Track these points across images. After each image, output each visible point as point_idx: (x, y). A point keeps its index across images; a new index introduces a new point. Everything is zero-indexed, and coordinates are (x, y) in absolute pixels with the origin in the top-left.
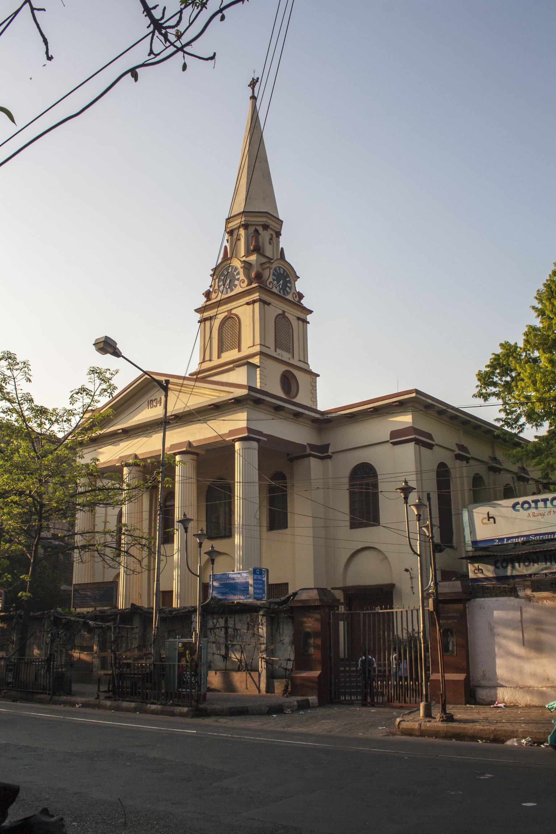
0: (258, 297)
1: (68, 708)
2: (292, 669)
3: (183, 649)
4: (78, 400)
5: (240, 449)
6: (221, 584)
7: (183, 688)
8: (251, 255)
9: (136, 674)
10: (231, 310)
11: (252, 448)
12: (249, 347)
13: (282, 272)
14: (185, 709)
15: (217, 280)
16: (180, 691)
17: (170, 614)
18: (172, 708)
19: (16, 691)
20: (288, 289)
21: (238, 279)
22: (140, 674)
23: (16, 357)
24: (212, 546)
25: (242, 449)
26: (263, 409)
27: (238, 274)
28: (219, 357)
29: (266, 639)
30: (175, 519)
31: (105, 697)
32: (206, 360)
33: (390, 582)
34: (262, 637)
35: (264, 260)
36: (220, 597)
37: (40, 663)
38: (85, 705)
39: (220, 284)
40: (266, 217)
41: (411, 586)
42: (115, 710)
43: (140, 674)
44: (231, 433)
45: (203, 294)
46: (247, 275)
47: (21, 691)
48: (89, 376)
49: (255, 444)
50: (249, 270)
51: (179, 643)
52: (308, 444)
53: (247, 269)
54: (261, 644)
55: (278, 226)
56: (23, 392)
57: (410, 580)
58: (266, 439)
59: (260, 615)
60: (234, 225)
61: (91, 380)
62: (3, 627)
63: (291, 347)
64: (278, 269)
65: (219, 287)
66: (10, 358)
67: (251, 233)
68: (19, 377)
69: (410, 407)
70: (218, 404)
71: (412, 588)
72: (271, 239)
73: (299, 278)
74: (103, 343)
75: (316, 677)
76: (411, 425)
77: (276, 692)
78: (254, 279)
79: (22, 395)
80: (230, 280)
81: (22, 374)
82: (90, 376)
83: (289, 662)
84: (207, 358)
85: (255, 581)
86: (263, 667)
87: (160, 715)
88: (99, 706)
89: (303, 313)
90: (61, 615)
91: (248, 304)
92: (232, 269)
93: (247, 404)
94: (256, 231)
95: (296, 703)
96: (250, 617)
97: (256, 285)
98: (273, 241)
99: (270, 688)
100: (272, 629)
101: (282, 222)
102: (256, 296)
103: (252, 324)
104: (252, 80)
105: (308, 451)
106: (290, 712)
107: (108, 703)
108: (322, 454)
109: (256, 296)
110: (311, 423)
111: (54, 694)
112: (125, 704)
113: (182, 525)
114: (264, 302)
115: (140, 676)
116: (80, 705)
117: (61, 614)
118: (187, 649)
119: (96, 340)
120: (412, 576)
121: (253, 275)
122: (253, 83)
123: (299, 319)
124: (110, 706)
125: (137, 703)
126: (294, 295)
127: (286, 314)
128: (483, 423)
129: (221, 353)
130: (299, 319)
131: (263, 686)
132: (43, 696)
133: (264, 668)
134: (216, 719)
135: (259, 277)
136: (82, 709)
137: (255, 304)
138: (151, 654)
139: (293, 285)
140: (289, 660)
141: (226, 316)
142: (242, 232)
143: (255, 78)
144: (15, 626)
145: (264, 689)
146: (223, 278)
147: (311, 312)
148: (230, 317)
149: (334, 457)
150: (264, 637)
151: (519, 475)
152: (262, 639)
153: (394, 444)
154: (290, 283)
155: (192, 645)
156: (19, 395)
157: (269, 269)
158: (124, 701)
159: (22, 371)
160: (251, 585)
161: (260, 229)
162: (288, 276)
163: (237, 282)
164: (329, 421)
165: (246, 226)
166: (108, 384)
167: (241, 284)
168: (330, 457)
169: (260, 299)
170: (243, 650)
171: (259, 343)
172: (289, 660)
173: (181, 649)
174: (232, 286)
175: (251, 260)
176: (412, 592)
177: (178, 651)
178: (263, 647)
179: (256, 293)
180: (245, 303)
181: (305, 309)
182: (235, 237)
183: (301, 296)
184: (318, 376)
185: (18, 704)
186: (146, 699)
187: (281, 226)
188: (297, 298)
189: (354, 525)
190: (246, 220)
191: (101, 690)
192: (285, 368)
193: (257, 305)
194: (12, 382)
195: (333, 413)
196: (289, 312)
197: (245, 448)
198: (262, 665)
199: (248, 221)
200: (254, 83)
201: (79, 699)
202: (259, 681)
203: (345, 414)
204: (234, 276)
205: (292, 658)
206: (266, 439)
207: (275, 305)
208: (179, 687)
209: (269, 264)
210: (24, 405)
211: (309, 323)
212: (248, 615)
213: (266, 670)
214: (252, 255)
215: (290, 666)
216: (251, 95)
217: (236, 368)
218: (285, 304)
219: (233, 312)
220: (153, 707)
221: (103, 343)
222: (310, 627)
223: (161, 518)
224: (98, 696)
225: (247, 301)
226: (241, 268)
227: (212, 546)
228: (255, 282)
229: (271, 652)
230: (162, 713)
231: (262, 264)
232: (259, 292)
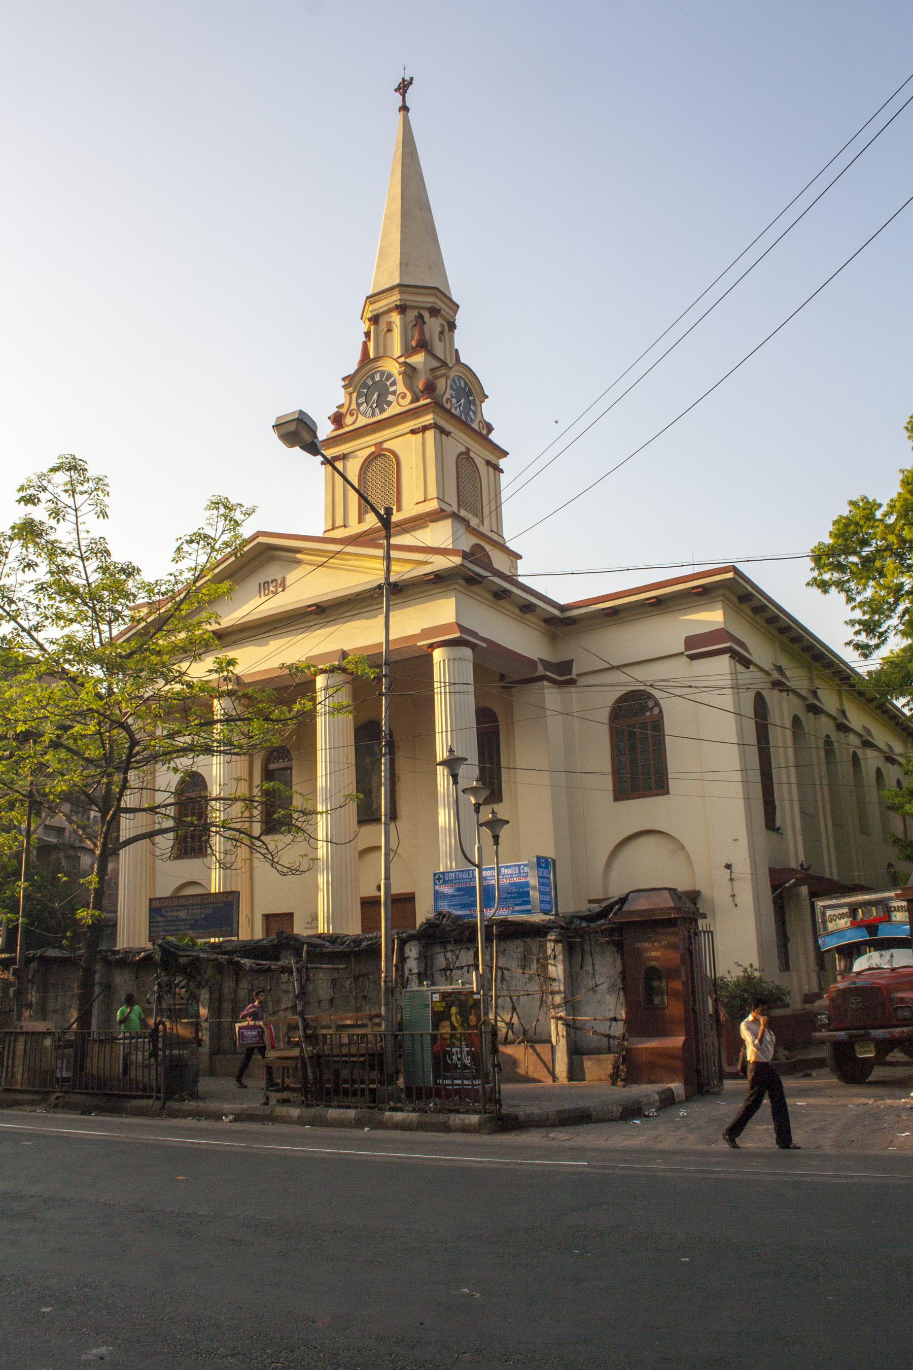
0: (432, 421)
1: (204, 1124)
3: (444, 1004)
4: (188, 556)
5: (444, 660)
6: (458, 890)
7: (446, 1078)
9: (344, 1056)
11: (465, 660)
12: (417, 503)
13: (463, 385)
14: (474, 1119)
15: (354, 395)
16: (439, 1084)
18: (442, 1117)
21: (394, 393)
22: (363, 1055)
23: (86, 466)
27: (394, 383)
28: (360, 521)
29: (564, 984)
31: (278, 1101)
34: (554, 980)
35: (435, 364)
36: (459, 913)
37: (127, 1041)
39: (360, 401)
41: (729, 892)
42: (313, 1126)
44: (426, 633)
45: (329, 418)
46: (410, 386)
48: (209, 513)
49: (468, 652)
50: (411, 378)
51: (432, 993)
52: (539, 659)
53: (408, 376)
54: (552, 993)
56: (90, 536)
58: (484, 645)
59: (550, 940)
60: (381, 308)
62: (7, 980)
63: (479, 508)
64: (456, 379)
65: (359, 405)
66: (75, 468)
67: (412, 321)
68: (85, 509)
71: (733, 896)
72: (442, 333)
73: (487, 397)
74: (295, 423)
75: (678, 1048)
76: (722, 626)
77: (587, 1078)
78: (422, 392)
79: (88, 541)
80: (379, 395)
81: (90, 502)
82: (211, 512)
84: (340, 522)
85: (541, 880)
86: (560, 1034)
87: (416, 1130)
88: (271, 1119)
89: (495, 455)
91: (413, 432)
92: (382, 377)
93: (457, 583)
94: (420, 317)
95: (657, 1097)
97: (428, 401)
98: (444, 336)
99: (575, 1073)
100: (571, 966)
101: (458, 306)
102: (428, 419)
103: (422, 465)
104: (401, 81)
105: (541, 671)
106: (656, 1114)
107: (295, 1112)
108: (561, 676)
109: (428, 419)
110: (542, 624)
111: (169, 1097)
112: (333, 1113)
115: (362, 1059)
116: (231, 1117)
118: (452, 1005)
119: (278, 418)
121: (421, 385)
122: (404, 87)
123: (488, 463)
125: (359, 1110)
127: (472, 454)
129: (364, 514)
130: (488, 463)
131: (561, 1067)
133: (563, 1036)
134: (544, 1135)
135: (430, 388)
136: (234, 1124)
137: (427, 432)
139: (479, 409)
140: (615, 1019)
141: (373, 453)
143: (407, 78)
144: (33, 976)
146: (365, 391)
147: (505, 454)
148: (380, 456)
149: (582, 681)
150: (559, 981)
151: (838, 722)
152: (555, 984)
153: (692, 657)
154: (475, 405)
155: (462, 997)
157: (444, 379)
158: (331, 1106)
159: (92, 496)
160: (534, 888)
161: (426, 315)
162: (470, 393)
163: (390, 398)
165: (402, 309)
167: (400, 399)
168: (572, 682)
169: (435, 423)
170: (516, 1004)
171: (436, 496)
173: (438, 1004)
174: (382, 403)
175: (414, 363)
177: (433, 1008)
178: (558, 999)
179: (427, 414)
180: (408, 430)
181: (497, 448)
182: (383, 326)
183: (490, 428)
185: (93, 1117)
186: (374, 1100)
189: (621, 793)
192: (475, 540)
193: (430, 434)
196: (476, 451)
198: (557, 1033)
200: (405, 86)
201: (227, 1107)
203: (603, 609)
204: (386, 388)
206: (484, 645)
208: (437, 1077)
209: (446, 369)
210: (90, 561)
211: (502, 472)
212: (519, 942)
213: (567, 1041)
214: (417, 354)
215: (618, 1029)
216: (400, 104)
219: (385, 445)
220: (399, 1116)
221: (295, 423)
222: (656, 959)
223: (388, 761)
225: (411, 428)
226: (399, 374)
229: (571, 1005)
230: (421, 1126)
231: (433, 370)
232: (433, 412)
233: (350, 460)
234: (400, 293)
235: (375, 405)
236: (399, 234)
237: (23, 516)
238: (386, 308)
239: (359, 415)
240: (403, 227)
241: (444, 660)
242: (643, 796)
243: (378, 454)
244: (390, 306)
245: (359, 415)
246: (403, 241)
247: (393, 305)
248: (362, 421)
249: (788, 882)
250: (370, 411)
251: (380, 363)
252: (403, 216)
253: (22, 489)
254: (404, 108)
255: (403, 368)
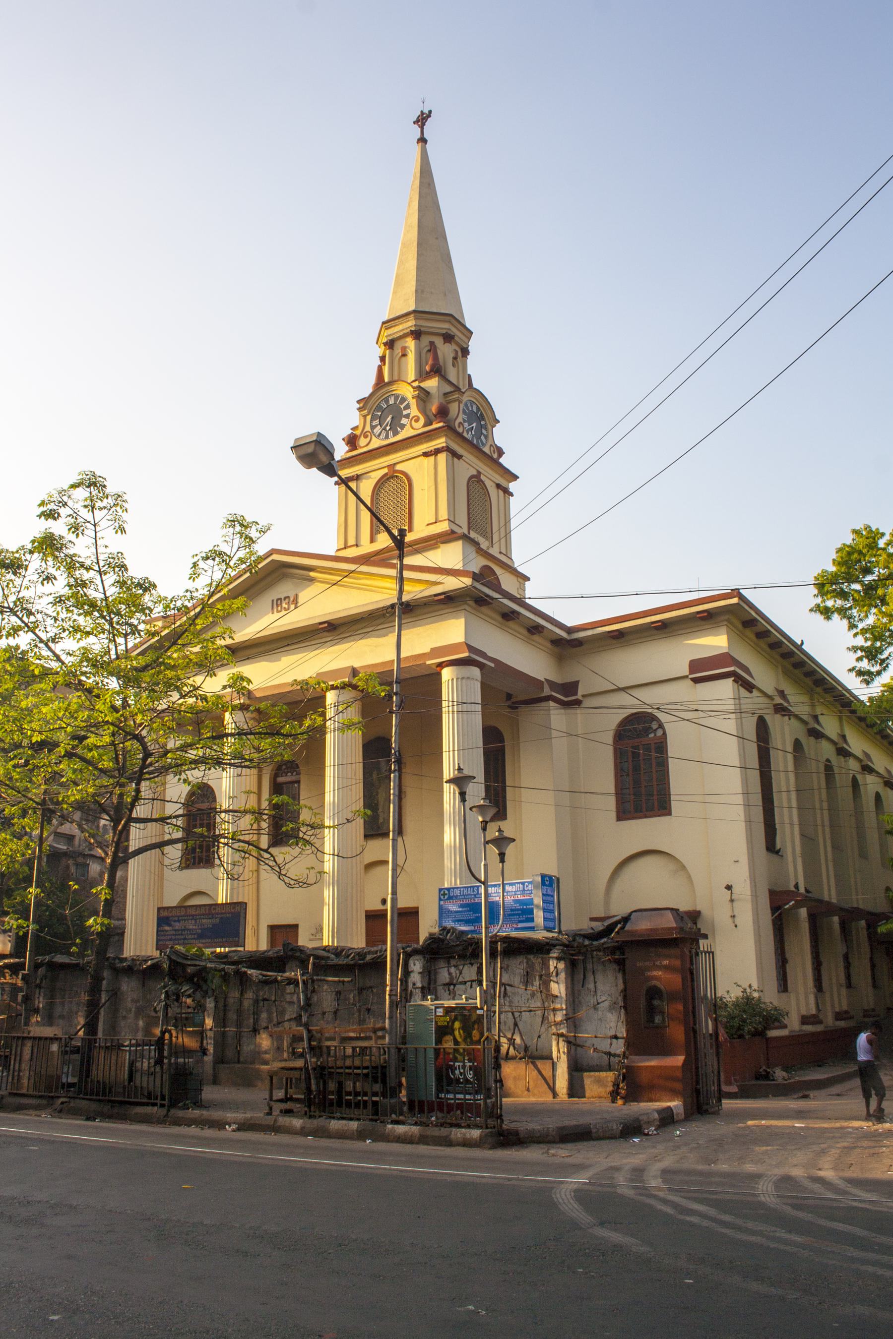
0: (444, 445)
1: (209, 1133)
2: (624, 1053)
4: (203, 572)
5: (453, 679)
7: (448, 1092)
8: (428, 379)
9: (358, 1068)
10: (395, 464)
12: (428, 525)
14: (476, 1133)
15: (369, 418)
16: (441, 1098)
17: (360, 960)
18: (444, 1131)
19: (87, 1099)
20: (482, 437)
21: (407, 416)
22: (367, 1068)
23: (105, 483)
24: (500, 829)
25: (457, 679)
26: (485, 615)
28: (372, 540)
30: (445, 777)
31: (281, 1111)
32: (349, 545)
33: (690, 909)
35: (448, 389)
38: (243, 1127)
39: (374, 424)
40: (450, 322)
41: (730, 914)
43: (367, 1068)
44: (436, 652)
45: (343, 439)
46: (423, 410)
47: (99, 1101)
48: (225, 530)
49: (476, 672)
50: (424, 402)
53: (422, 400)
55: (466, 340)
56: (108, 550)
57: (729, 905)
58: (492, 665)
59: (553, 958)
61: (227, 539)
62: (16, 984)
63: (489, 530)
65: (373, 427)
66: (94, 484)
68: (103, 524)
69: (723, 621)
70: (334, 622)
71: (733, 916)
72: (455, 358)
74: (314, 443)
77: (587, 1095)
78: (435, 416)
79: (106, 555)
83: (614, 1040)
84: (352, 541)
85: (545, 898)
87: (417, 1143)
88: (276, 1129)
89: (505, 478)
90: (186, 959)
91: (426, 454)
93: (466, 604)
95: (656, 1116)
96: (527, 963)
97: (441, 424)
98: (458, 363)
99: (575, 1089)
101: (471, 333)
102: (441, 442)
103: (434, 487)
106: (655, 1132)
107: (297, 1123)
109: (441, 442)
111: (173, 1104)
112: (335, 1125)
113: (456, 789)
114: (454, 454)
115: (365, 1071)
116: (234, 1127)
117: (185, 957)
120: (733, 897)
122: (422, 120)
123: (498, 486)
124: (303, 1128)
126: (492, 449)
127: (483, 478)
128: (807, 658)
129: (376, 534)
130: (498, 486)
131: (562, 1083)
132: (149, 1109)
135: (443, 412)
138: (383, 1029)
139: (490, 433)
141: (386, 474)
142: (411, 343)
145: (565, 1091)
146: (379, 413)
147: (515, 477)
148: (392, 477)
153: (696, 681)
154: (486, 429)
156: (101, 557)
158: (334, 1118)
159: (111, 512)
161: (439, 342)
162: (482, 418)
164: (579, 643)
165: (417, 334)
166: (248, 550)
168: (578, 703)
169: (447, 447)
172: (616, 1037)
173: (442, 1019)
174: (396, 426)
176: (734, 925)
177: (436, 1022)
178: (559, 1017)
180: (421, 453)
183: (501, 452)
184: (528, 579)
185: (97, 1123)
186: (377, 1112)
187: (469, 339)
188: (496, 454)
189: (624, 813)
190: (418, 324)
191: (274, 1098)
193: (442, 457)
194: (90, 532)
195: (589, 629)
197: (463, 678)
198: (559, 1051)
199: (421, 326)
200: (423, 119)
201: (230, 1116)
202: (554, 1076)
203: (609, 632)
205: (622, 1032)
206: (492, 665)
207: (467, 460)
208: (439, 1089)
214: (431, 379)
215: (619, 1047)
216: (419, 136)
217: (441, 545)
218: (479, 460)
219: (398, 467)
220: (401, 1129)
221: (314, 443)
224: (271, 1108)
225: (424, 451)
226: (413, 398)
227: (500, 829)
228: (438, 421)
230: (423, 1140)
231: (446, 394)
232: (446, 435)
233: (364, 481)
234: (416, 319)
235: (388, 428)
236: (416, 262)
237: (43, 530)
238: (401, 334)
239: (373, 437)
240: (419, 255)
241: (453, 679)
242: (646, 817)
243: (392, 476)
244: (405, 331)
245: (373, 437)
246: (419, 269)
247: (408, 330)
248: (376, 443)
249: (788, 904)
250: (384, 434)
251: (394, 387)
252: (420, 244)
253: (43, 504)
254: (423, 140)
255: (417, 392)
